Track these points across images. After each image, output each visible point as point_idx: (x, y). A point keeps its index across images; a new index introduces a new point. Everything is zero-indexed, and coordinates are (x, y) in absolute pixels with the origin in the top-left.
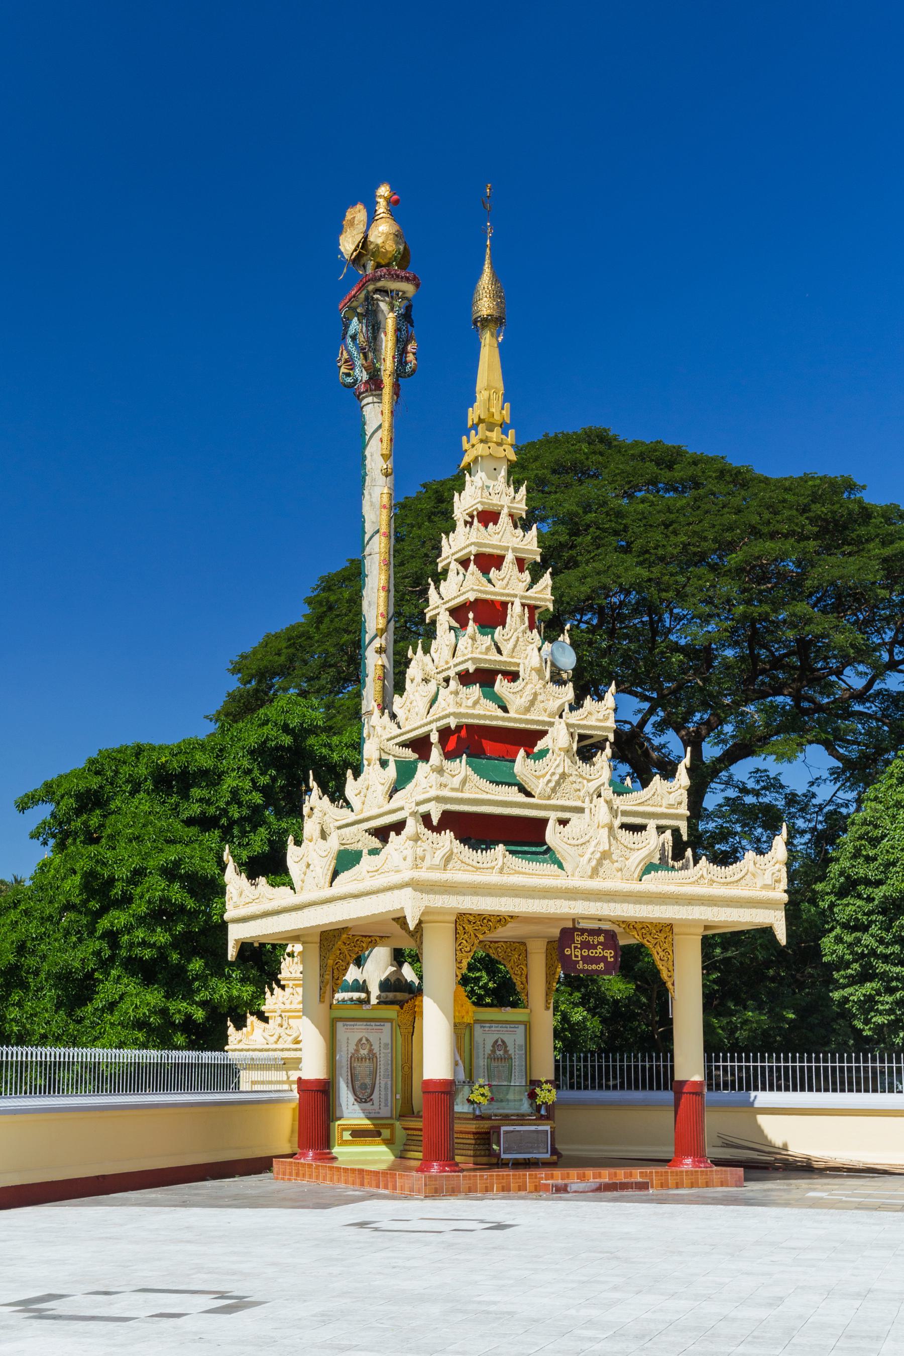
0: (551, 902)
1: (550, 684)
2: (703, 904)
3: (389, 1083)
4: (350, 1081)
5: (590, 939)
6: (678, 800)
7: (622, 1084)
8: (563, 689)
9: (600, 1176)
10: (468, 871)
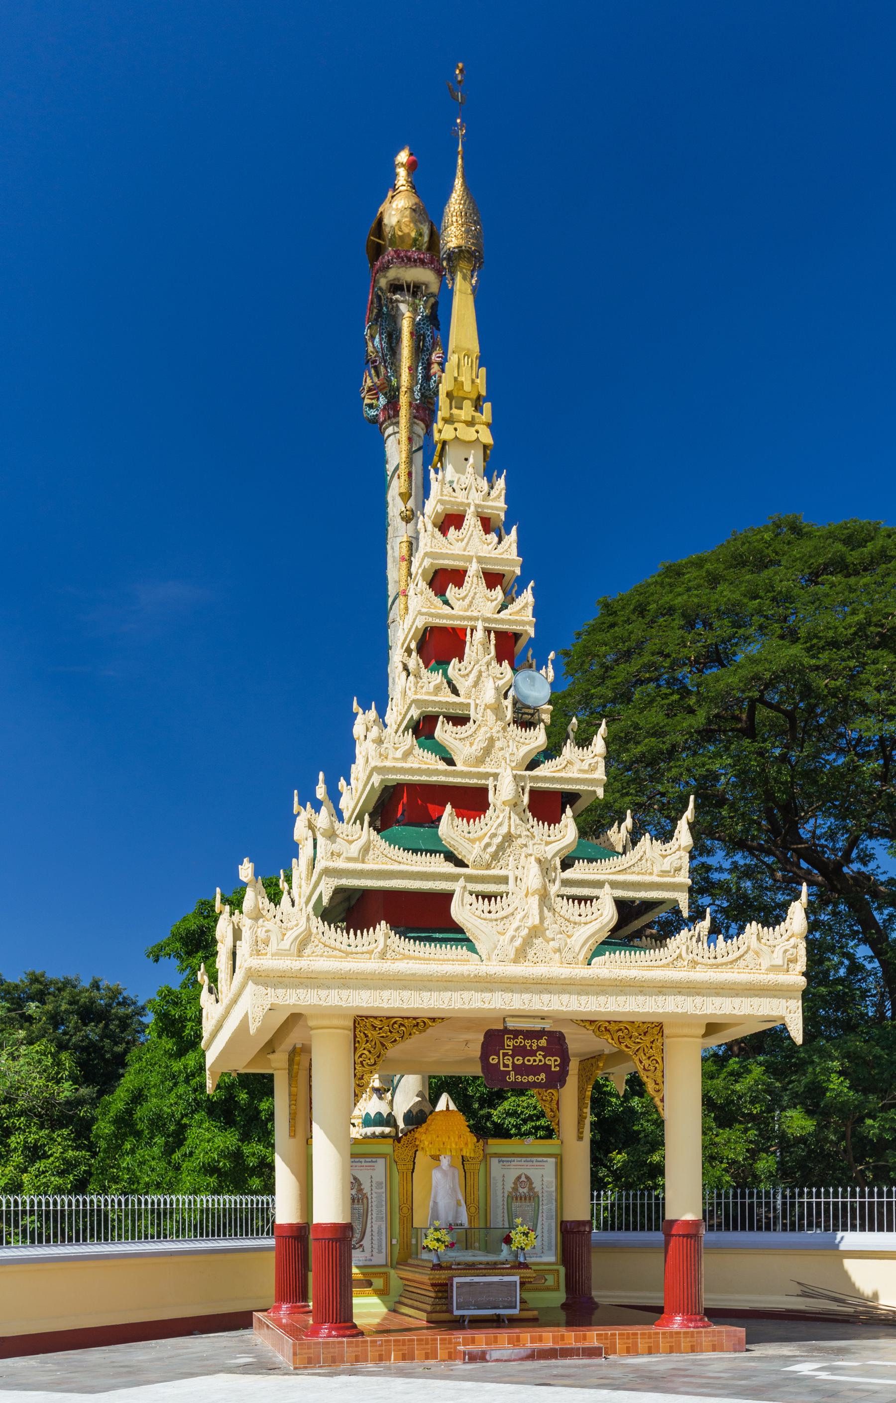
0: (456, 995)
1: (513, 727)
2: (680, 993)
3: (383, 1227)
5: (527, 1043)
6: (676, 864)
7: (793, 1224)
8: (531, 733)
9: (540, 1339)
10: (335, 957)
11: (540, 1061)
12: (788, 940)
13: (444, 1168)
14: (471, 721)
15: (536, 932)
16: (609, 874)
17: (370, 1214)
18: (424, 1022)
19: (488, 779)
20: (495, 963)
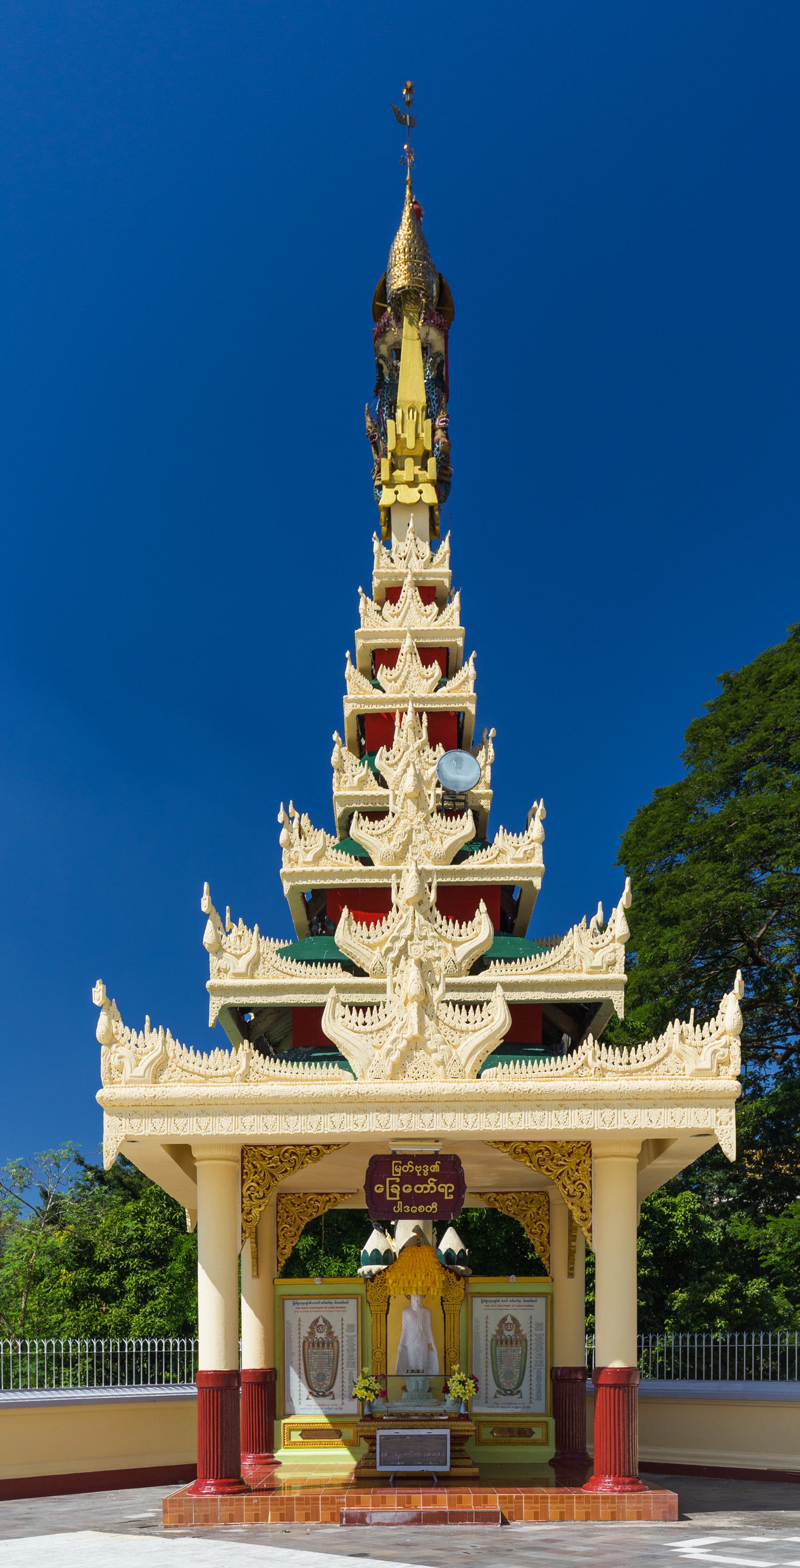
0: (326, 1118)
4: (303, 1371)
5: (418, 1169)
6: (609, 958)
8: (457, 822)
9: (434, 1500)
10: (194, 1081)
11: (432, 1188)
12: (718, 1039)
13: (414, 1309)
14: (390, 814)
15: (416, 1044)
16: (530, 974)
17: (340, 1358)
18: (318, 1150)
19: (389, 877)
20: (369, 1081)
